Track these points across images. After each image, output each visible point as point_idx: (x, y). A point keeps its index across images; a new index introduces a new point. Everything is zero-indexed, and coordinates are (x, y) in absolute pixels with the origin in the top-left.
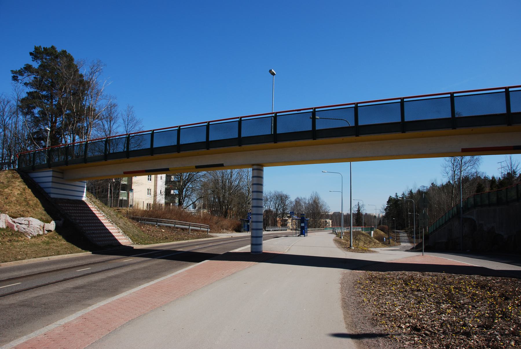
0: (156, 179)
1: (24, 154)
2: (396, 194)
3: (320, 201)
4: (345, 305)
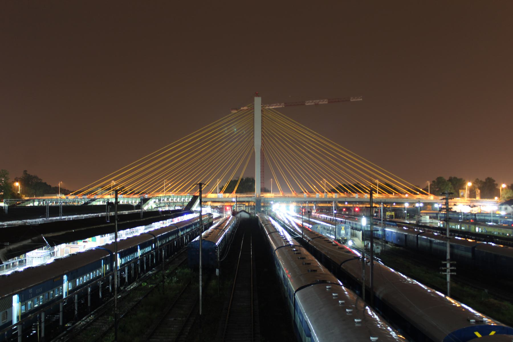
1: (122, 191)
2: (461, 210)
4: (39, 265)
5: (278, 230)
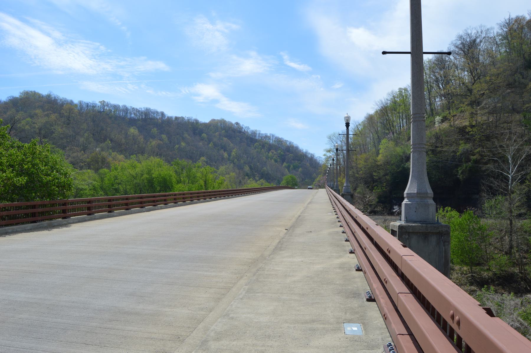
0: (375, 270)
3: (36, 92)
4: (103, 103)
5: (60, 228)
